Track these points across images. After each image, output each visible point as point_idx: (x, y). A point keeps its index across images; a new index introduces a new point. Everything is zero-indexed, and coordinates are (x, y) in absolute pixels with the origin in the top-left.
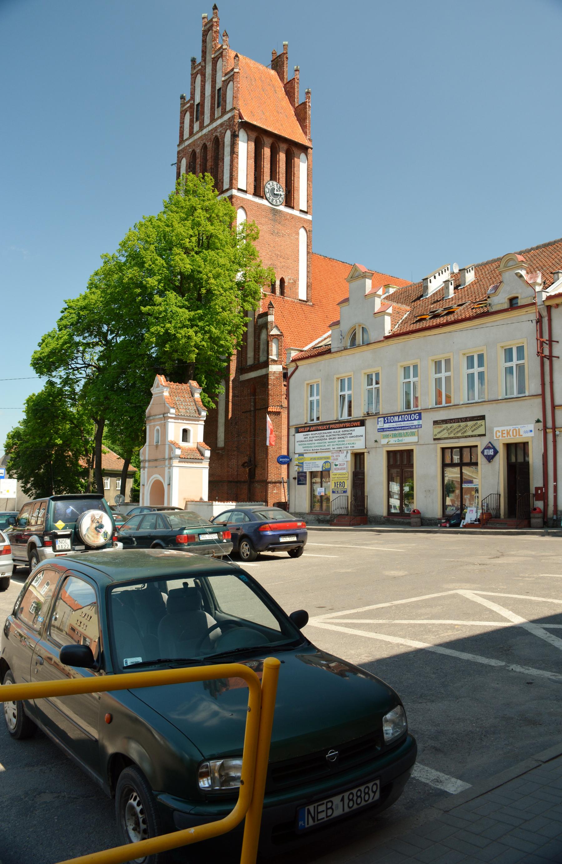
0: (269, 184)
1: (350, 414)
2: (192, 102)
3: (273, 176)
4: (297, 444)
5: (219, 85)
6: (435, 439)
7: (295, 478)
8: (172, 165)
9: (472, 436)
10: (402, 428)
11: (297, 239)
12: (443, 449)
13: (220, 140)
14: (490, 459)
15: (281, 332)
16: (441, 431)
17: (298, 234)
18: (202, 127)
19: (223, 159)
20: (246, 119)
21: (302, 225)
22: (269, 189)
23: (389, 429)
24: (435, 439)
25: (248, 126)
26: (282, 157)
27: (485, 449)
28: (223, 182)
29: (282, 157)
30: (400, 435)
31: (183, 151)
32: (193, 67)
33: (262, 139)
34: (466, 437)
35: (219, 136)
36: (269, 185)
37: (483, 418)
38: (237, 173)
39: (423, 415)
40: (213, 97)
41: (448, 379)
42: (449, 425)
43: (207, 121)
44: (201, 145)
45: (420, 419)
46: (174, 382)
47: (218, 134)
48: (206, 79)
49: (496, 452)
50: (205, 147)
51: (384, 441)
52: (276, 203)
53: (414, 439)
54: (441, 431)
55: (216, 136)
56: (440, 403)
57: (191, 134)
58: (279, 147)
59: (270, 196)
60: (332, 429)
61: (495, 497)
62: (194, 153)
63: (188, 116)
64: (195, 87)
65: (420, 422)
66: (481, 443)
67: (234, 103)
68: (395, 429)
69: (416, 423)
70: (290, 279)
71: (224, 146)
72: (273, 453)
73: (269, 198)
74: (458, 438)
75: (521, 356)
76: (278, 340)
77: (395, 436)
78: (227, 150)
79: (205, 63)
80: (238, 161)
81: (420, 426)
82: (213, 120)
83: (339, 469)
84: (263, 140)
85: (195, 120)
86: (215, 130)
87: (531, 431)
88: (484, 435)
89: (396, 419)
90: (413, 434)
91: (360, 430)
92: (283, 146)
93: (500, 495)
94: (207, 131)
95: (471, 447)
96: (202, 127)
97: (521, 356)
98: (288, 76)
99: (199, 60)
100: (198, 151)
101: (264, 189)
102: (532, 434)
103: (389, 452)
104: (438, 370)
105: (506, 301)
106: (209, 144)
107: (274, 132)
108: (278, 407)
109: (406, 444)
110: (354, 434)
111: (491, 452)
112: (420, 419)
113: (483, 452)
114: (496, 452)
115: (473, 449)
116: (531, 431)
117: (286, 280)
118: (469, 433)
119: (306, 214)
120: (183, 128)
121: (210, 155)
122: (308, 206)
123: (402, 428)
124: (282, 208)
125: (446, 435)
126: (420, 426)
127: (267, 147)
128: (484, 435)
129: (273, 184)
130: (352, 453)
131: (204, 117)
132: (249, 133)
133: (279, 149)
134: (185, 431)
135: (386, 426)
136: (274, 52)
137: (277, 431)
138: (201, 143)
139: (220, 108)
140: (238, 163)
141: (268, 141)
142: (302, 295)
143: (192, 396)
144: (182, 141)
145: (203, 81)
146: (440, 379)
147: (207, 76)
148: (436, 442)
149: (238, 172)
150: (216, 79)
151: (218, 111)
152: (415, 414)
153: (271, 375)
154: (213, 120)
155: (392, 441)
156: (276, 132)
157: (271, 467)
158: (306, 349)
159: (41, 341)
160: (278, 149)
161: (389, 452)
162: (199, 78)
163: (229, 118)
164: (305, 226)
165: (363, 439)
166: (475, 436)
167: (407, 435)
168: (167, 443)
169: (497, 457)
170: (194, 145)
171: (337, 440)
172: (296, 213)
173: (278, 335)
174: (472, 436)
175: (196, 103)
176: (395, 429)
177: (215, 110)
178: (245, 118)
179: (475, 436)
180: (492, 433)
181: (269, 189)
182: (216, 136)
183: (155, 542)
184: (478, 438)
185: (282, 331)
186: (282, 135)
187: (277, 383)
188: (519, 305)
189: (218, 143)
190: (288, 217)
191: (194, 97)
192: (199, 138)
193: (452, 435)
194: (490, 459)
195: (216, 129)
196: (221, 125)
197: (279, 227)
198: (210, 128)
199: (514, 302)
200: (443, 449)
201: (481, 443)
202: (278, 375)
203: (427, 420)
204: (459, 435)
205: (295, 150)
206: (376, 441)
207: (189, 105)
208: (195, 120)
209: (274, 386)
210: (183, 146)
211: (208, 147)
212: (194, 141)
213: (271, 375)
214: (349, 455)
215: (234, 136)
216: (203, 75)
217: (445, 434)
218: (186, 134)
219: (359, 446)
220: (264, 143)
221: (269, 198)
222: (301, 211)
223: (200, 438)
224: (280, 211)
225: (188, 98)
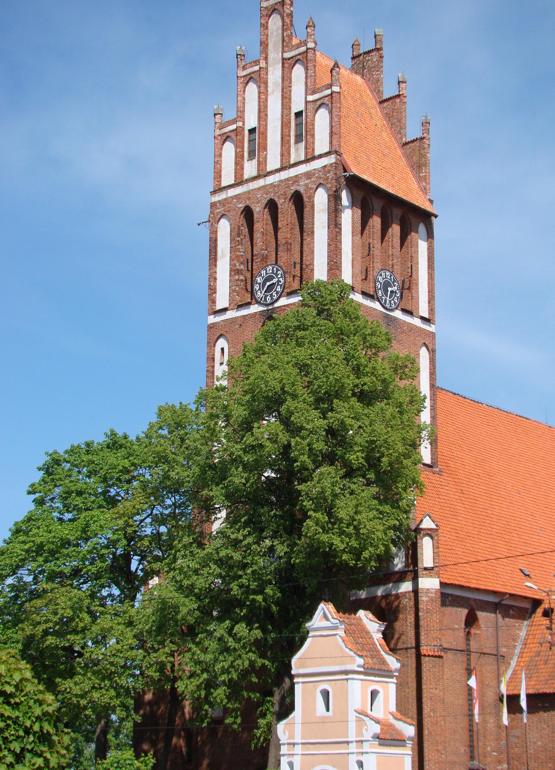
0: (381, 275)
2: (240, 124)
5: (297, 105)
8: (199, 224)
13: (305, 199)
15: (437, 525)
19: (313, 232)
20: (355, 170)
21: (423, 341)
22: (381, 283)
31: (224, 205)
33: (370, 201)
35: (302, 191)
38: (341, 258)
40: (285, 125)
43: (274, 162)
44: (265, 202)
46: (344, 613)
47: (302, 190)
48: (270, 90)
52: (390, 306)
57: (239, 182)
58: (392, 214)
59: (383, 296)
64: (244, 99)
67: (334, 143)
71: (313, 210)
72: (431, 726)
73: (381, 297)
76: (432, 538)
79: (267, 63)
80: (341, 238)
84: (372, 202)
85: (246, 155)
86: (295, 182)
87: (374, 694)
92: (397, 212)
94: (277, 180)
98: (389, 91)
100: (258, 209)
107: (388, 190)
108: (436, 648)
119: (428, 323)
120: (220, 164)
122: (432, 310)
127: (377, 215)
129: (386, 274)
131: (266, 154)
132: (355, 193)
133: (392, 218)
136: (356, 43)
137: (436, 689)
139: (302, 145)
140: (341, 242)
141: (377, 204)
143: (504, 646)
147: (270, 84)
149: (341, 255)
150: (290, 95)
151: (297, 150)
153: (422, 595)
156: (390, 191)
157: (429, 750)
160: (390, 217)
163: (325, 167)
164: (427, 343)
170: (249, 199)
172: (417, 322)
173: (430, 529)
175: (248, 127)
177: (290, 147)
178: (353, 170)
181: (381, 283)
185: (439, 524)
186: (399, 195)
187: (433, 608)
190: (405, 328)
191: (244, 116)
192: (259, 189)
195: (296, 179)
196: (308, 175)
202: (433, 595)
205: (412, 219)
208: (246, 155)
209: (427, 612)
211: (279, 207)
212: (249, 192)
213: (422, 595)
218: (228, 179)
220: (373, 208)
221: (381, 297)
222: (422, 318)
224: (395, 319)
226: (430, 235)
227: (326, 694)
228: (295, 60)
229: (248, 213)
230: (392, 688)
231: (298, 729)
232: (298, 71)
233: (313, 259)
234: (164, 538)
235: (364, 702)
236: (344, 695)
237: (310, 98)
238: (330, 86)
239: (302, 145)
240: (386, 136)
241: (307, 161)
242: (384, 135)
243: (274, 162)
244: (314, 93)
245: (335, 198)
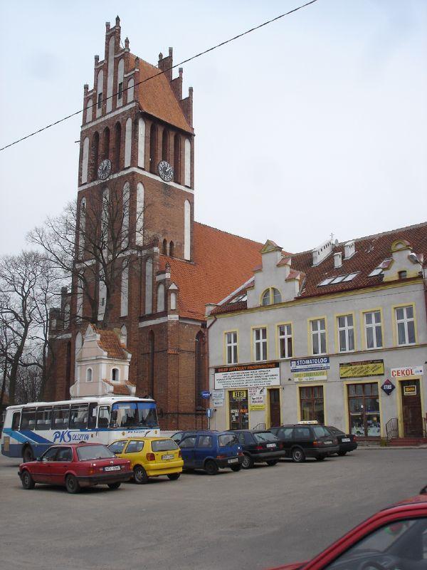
1: (236, 361)
3: (164, 159)
4: (216, 382)
5: (120, 80)
6: (341, 378)
7: (123, 434)
9: (373, 375)
10: (312, 369)
11: (183, 210)
12: (348, 385)
14: (388, 392)
16: (347, 372)
17: (184, 205)
18: (104, 114)
20: (145, 110)
23: (301, 370)
24: (341, 378)
25: (147, 117)
26: (171, 140)
27: (385, 384)
28: (124, 161)
29: (171, 140)
30: (311, 375)
32: (97, 64)
34: (368, 376)
36: (163, 164)
37: (382, 361)
39: (330, 359)
41: (351, 332)
42: (353, 367)
43: (109, 108)
45: (328, 362)
47: (120, 121)
48: (109, 74)
49: (393, 387)
50: (107, 130)
51: (296, 380)
53: (325, 377)
54: (347, 372)
55: (118, 122)
56: (372, 346)
57: (94, 119)
60: (249, 369)
61: (394, 421)
62: (97, 135)
63: (90, 103)
65: (329, 365)
66: (380, 381)
68: (307, 370)
69: (324, 365)
70: (177, 243)
74: (361, 377)
75: (410, 315)
76: (176, 294)
77: (307, 375)
78: (128, 135)
81: (328, 368)
82: (115, 109)
83: (256, 402)
87: (421, 371)
88: (383, 374)
89: (308, 362)
90: (323, 374)
91: (275, 371)
93: (397, 420)
95: (371, 384)
96: (104, 114)
97: (410, 315)
99: (102, 58)
101: (158, 167)
102: (422, 373)
103: (301, 389)
104: (342, 324)
105: (397, 274)
106: (111, 128)
109: (317, 381)
110: (270, 373)
111: (389, 387)
112: (328, 362)
113: (382, 388)
114: (393, 387)
115: (373, 385)
116: (421, 371)
117: (175, 243)
118: (371, 373)
121: (112, 137)
123: (312, 369)
124: (172, 184)
125: (351, 375)
126: (328, 368)
128: (383, 374)
130: (268, 389)
134: (114, 371)
135: (299, 367)
138: (104, 126)
142: (187, 256)
144: (85, 123)
145: (106, 76)
146: (403, 324)
147: (109, 71)
148: (342, 380)
152: (323, 358)
154: (115, 109)
155: (304, 379)
158: (220, 304)
159: (248, 292)
161: (301, 389)
162: (101, 73)
165: (278, 377)
166: (375, 375)
167: (317, 374)
168: (100, 380)
169: (394, 392)
171: (254, 378)
174: (373, 375)
176: (307, 370)
179: (375, 375)
180: (389, 372)
182: (118, 122)
183: (67, 472)
184: (378, 377)
188: (407, 277)
189: (119, 128)
193: (356, 375)
194: (388, 392)
195: (118, 116)
196: (123, 113)
197: (170, 199)
198: (112, 115)
199: (403, 274)
200: (348, 385)
201: (380, 381)
203: (334, 363)
204: (361, 374)
206: (290, 380)
207: (92, 94)
210: (87, 128)
214: (265, 392)
215: (135, 124)
216: (106, 71)
217: (350, 374)
218: (89, 118)
219: (275, 383)
222: (186, 186)
223: (126, 377)
225: (91, 87)
226: (346, 242)
227: (90, 370)
228: (120, 58)
229: (97, 135)
230: (126, 369)
231: (78, 389)
232: (122, 63)
233: (124, 155)
234: (70, 291)
235: (108, 374)
236: (98, 372)
237: (126, 76)
238: (134, 69)
239: (122, 99)
240: (171, 97)
241: (124, 106)
242: (170, 97)
243: (109, 108)
244: (127, 73)
245: (135, 124)
